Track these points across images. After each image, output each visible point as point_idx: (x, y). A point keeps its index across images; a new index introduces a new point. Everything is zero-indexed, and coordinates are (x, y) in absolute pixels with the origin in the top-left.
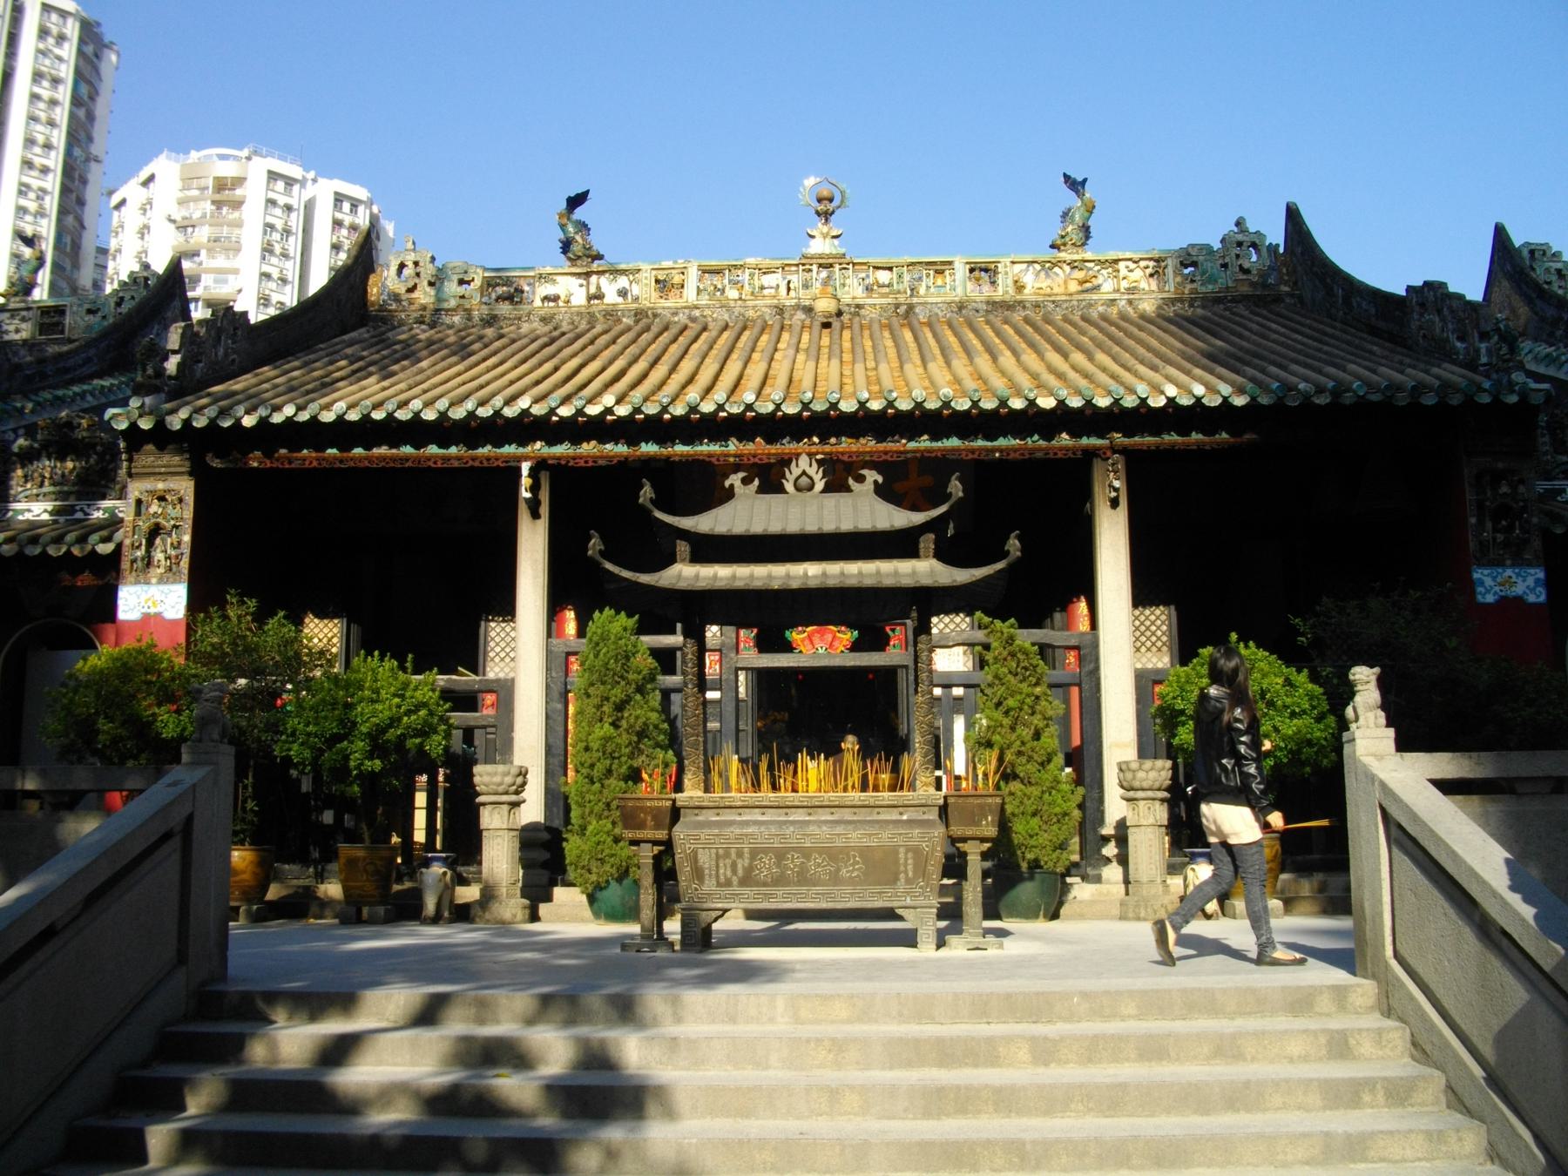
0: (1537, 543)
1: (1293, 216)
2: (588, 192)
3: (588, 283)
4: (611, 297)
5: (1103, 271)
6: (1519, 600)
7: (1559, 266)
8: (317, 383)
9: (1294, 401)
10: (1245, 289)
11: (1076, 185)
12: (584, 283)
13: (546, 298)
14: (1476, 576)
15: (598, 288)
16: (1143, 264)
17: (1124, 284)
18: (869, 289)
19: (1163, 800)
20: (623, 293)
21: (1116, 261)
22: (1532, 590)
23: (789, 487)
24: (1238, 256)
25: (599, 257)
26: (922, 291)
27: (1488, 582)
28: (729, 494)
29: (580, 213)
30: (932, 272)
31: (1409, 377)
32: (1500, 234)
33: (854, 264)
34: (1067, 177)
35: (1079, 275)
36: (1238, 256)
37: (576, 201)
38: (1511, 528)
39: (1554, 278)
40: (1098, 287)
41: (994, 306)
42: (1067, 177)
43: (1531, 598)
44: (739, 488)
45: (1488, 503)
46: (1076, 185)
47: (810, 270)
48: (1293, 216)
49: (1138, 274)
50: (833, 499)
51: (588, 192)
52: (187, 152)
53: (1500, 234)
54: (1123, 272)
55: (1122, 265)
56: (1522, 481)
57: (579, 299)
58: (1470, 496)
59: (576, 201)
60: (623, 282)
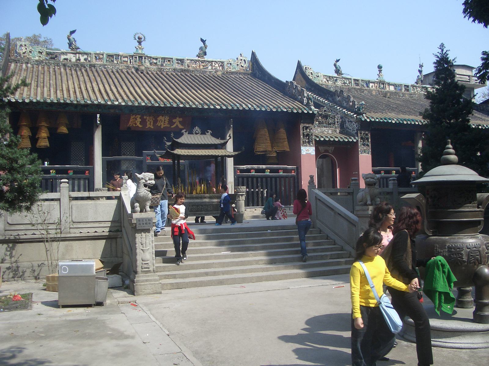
0: (314, 142)
1: (253, 54)
2: (76, 30)
3: (76, 56)
4: (82, 60)
5: (209, 64)
6: (310, 154)
7: (311, 71)
8: (39, 89)
9: (269, 110)
10: (242, 71)
11: (203, 41)
12: (75, 55)
13: (65, 59)
14: (302, 148)
15: (79, 57)
16: (218, 63)
17: (214, 67)
18: (151, 64)
19: (417, 225)
20: (85, 59)
21: (212, 61)
22: (312, 152)
23: (194, 133)
24: (241, 63)
25: (79, 48)
26: (164, 65)
27: (304, 150)
28: (182, 134)
29: (73, 36)
30: (167, 61)
31: (291, 105)
32: (299, 63)
33: (148, 57)
34: (201, 39)
35: (203, 64)
36: (241, 63)
37: (72, 32)
38: (309, 139)
39: (310, 74)
40: (208, 68)
41: (182, 70)
42: (201, 39)
43: (312, 154)
44: (184, 133)
45: (305, 133)
46: (203, 41)
47: (137, 58)
48: (253, 54)
49: (217, 65)
50: (202, 136)
51: (76, 30)
52: (477, 226)
53: (299, 63)
54: (214, 64)
55: (213, 63)
56: (311, 129)
57: (74, 60)
58: (301, 132)
59: (72, 32)
60: (86, 57)
